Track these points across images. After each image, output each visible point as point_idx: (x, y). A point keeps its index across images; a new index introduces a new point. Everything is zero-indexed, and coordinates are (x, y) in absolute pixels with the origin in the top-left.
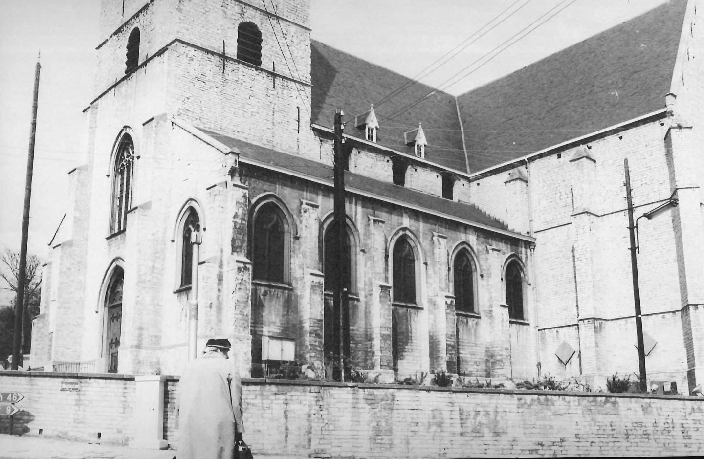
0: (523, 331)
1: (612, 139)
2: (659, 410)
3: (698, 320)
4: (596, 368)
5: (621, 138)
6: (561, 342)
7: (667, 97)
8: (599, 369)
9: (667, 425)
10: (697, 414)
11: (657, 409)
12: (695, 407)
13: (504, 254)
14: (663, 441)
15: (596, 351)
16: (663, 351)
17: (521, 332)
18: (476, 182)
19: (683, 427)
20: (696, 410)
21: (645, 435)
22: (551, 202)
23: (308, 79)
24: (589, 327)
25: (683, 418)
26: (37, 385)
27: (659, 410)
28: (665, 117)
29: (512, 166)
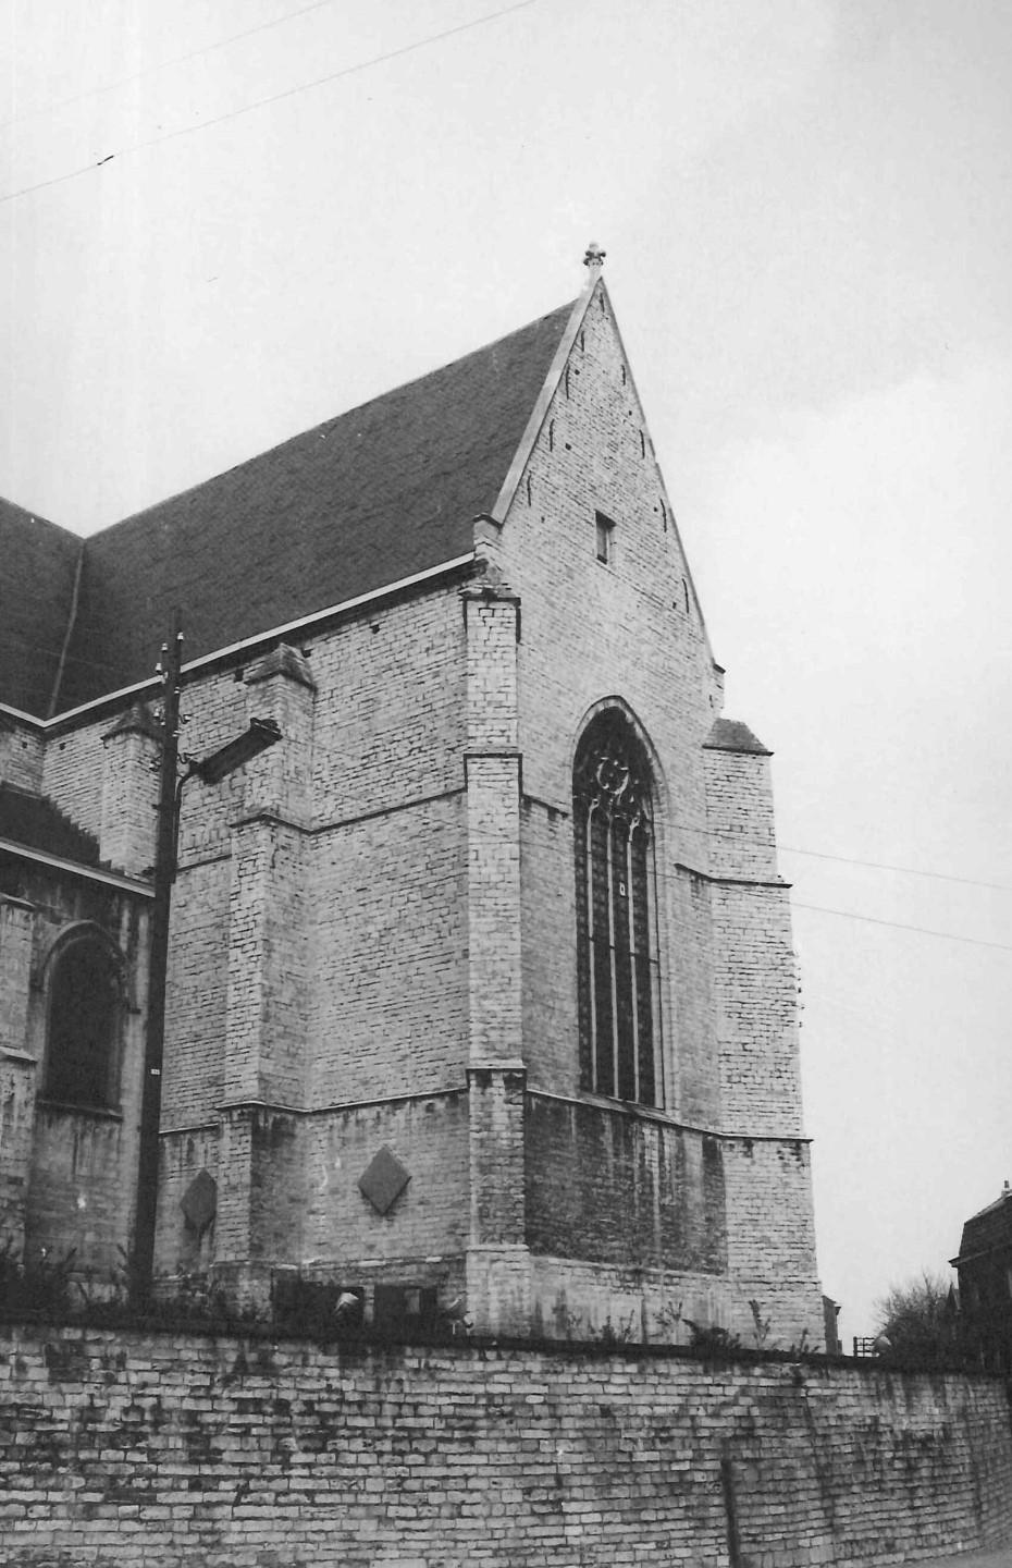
0: (95, 1136)
1: (357, 634)
2: (113, 1365)
3: (489, 1115)
4: (246, 1246)
5: (376, 629)
6: (197, 1173)
7: (477, 525)
8: (256, 1249)
9: (133, 1418)
10: (256, 1382)
11: (105, 1360)
12: (252, 1357)
13: (57, 921)
14: (111, 1470)
15: (252, 1199)
16: (421, 1203)
17: (88, 1141)
18: (56, 743)
19: (197, 1423)
20: (251, 1369)
21: (43, 1447)
22: (210, 795)
23: (564, 799)
24: (241, 1131)
25: (202, 1393)
26: (538, 1308)
27: (113, 1365)
28: (472, 576)
29: (126, 702)
